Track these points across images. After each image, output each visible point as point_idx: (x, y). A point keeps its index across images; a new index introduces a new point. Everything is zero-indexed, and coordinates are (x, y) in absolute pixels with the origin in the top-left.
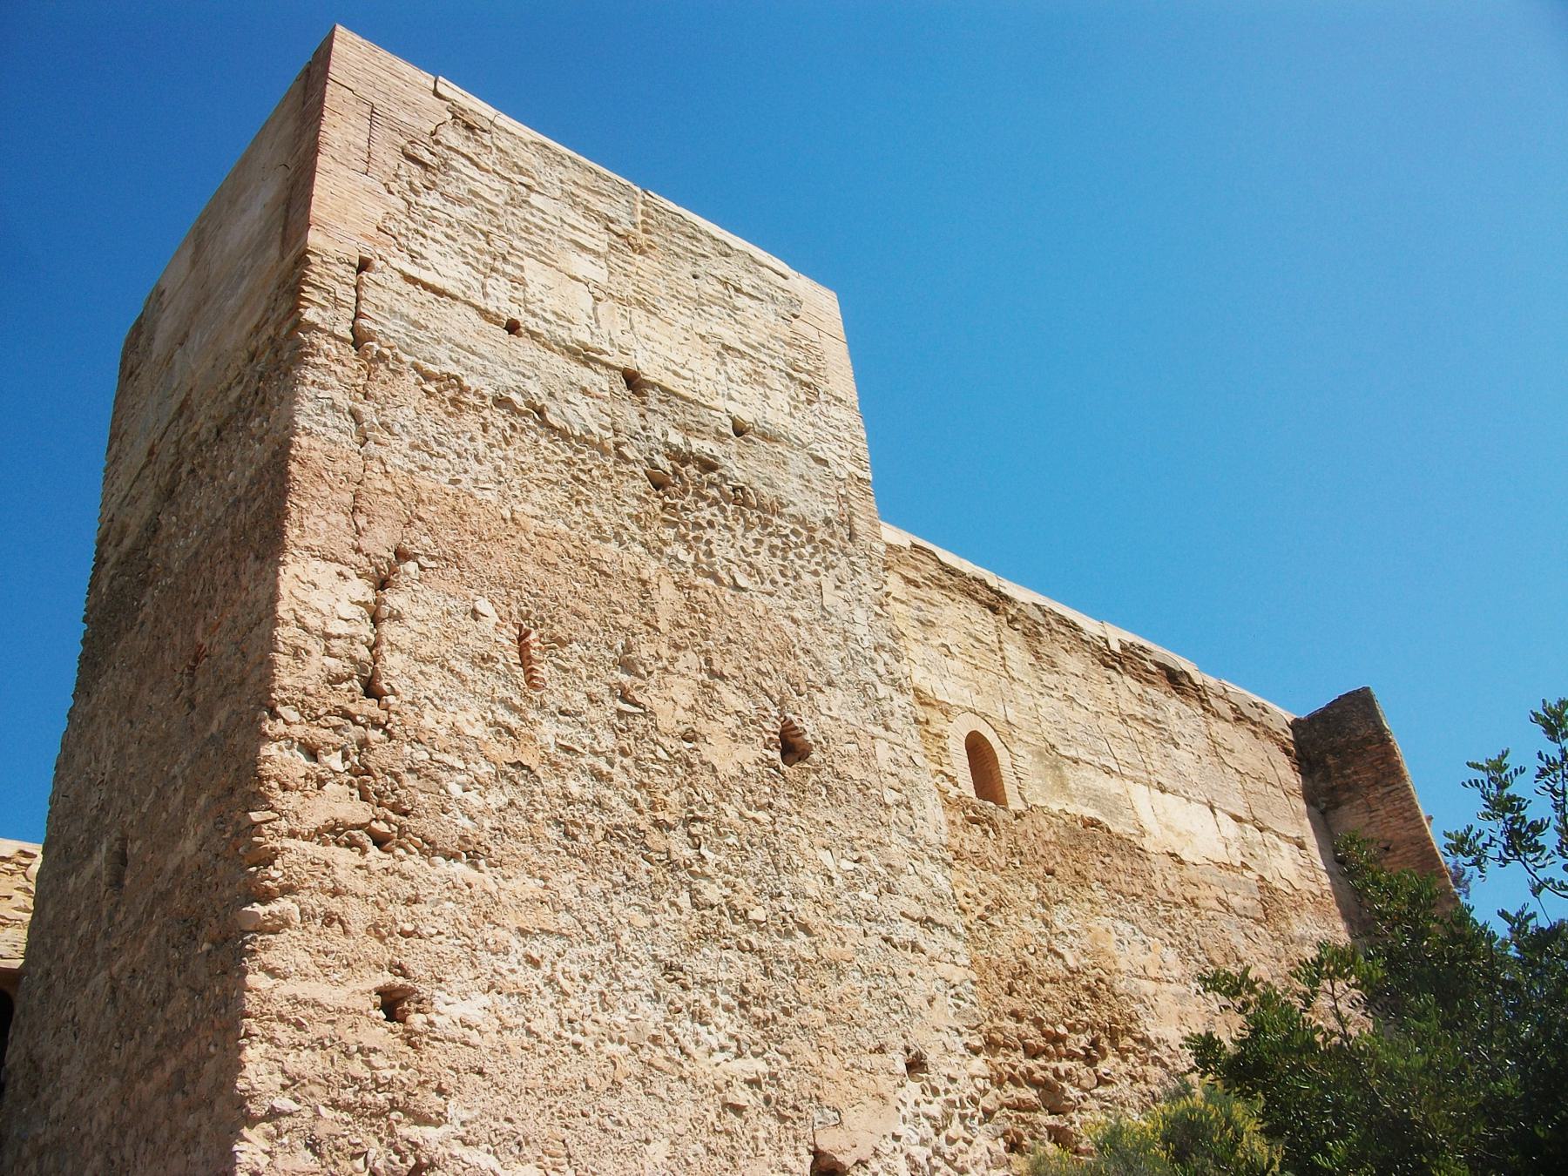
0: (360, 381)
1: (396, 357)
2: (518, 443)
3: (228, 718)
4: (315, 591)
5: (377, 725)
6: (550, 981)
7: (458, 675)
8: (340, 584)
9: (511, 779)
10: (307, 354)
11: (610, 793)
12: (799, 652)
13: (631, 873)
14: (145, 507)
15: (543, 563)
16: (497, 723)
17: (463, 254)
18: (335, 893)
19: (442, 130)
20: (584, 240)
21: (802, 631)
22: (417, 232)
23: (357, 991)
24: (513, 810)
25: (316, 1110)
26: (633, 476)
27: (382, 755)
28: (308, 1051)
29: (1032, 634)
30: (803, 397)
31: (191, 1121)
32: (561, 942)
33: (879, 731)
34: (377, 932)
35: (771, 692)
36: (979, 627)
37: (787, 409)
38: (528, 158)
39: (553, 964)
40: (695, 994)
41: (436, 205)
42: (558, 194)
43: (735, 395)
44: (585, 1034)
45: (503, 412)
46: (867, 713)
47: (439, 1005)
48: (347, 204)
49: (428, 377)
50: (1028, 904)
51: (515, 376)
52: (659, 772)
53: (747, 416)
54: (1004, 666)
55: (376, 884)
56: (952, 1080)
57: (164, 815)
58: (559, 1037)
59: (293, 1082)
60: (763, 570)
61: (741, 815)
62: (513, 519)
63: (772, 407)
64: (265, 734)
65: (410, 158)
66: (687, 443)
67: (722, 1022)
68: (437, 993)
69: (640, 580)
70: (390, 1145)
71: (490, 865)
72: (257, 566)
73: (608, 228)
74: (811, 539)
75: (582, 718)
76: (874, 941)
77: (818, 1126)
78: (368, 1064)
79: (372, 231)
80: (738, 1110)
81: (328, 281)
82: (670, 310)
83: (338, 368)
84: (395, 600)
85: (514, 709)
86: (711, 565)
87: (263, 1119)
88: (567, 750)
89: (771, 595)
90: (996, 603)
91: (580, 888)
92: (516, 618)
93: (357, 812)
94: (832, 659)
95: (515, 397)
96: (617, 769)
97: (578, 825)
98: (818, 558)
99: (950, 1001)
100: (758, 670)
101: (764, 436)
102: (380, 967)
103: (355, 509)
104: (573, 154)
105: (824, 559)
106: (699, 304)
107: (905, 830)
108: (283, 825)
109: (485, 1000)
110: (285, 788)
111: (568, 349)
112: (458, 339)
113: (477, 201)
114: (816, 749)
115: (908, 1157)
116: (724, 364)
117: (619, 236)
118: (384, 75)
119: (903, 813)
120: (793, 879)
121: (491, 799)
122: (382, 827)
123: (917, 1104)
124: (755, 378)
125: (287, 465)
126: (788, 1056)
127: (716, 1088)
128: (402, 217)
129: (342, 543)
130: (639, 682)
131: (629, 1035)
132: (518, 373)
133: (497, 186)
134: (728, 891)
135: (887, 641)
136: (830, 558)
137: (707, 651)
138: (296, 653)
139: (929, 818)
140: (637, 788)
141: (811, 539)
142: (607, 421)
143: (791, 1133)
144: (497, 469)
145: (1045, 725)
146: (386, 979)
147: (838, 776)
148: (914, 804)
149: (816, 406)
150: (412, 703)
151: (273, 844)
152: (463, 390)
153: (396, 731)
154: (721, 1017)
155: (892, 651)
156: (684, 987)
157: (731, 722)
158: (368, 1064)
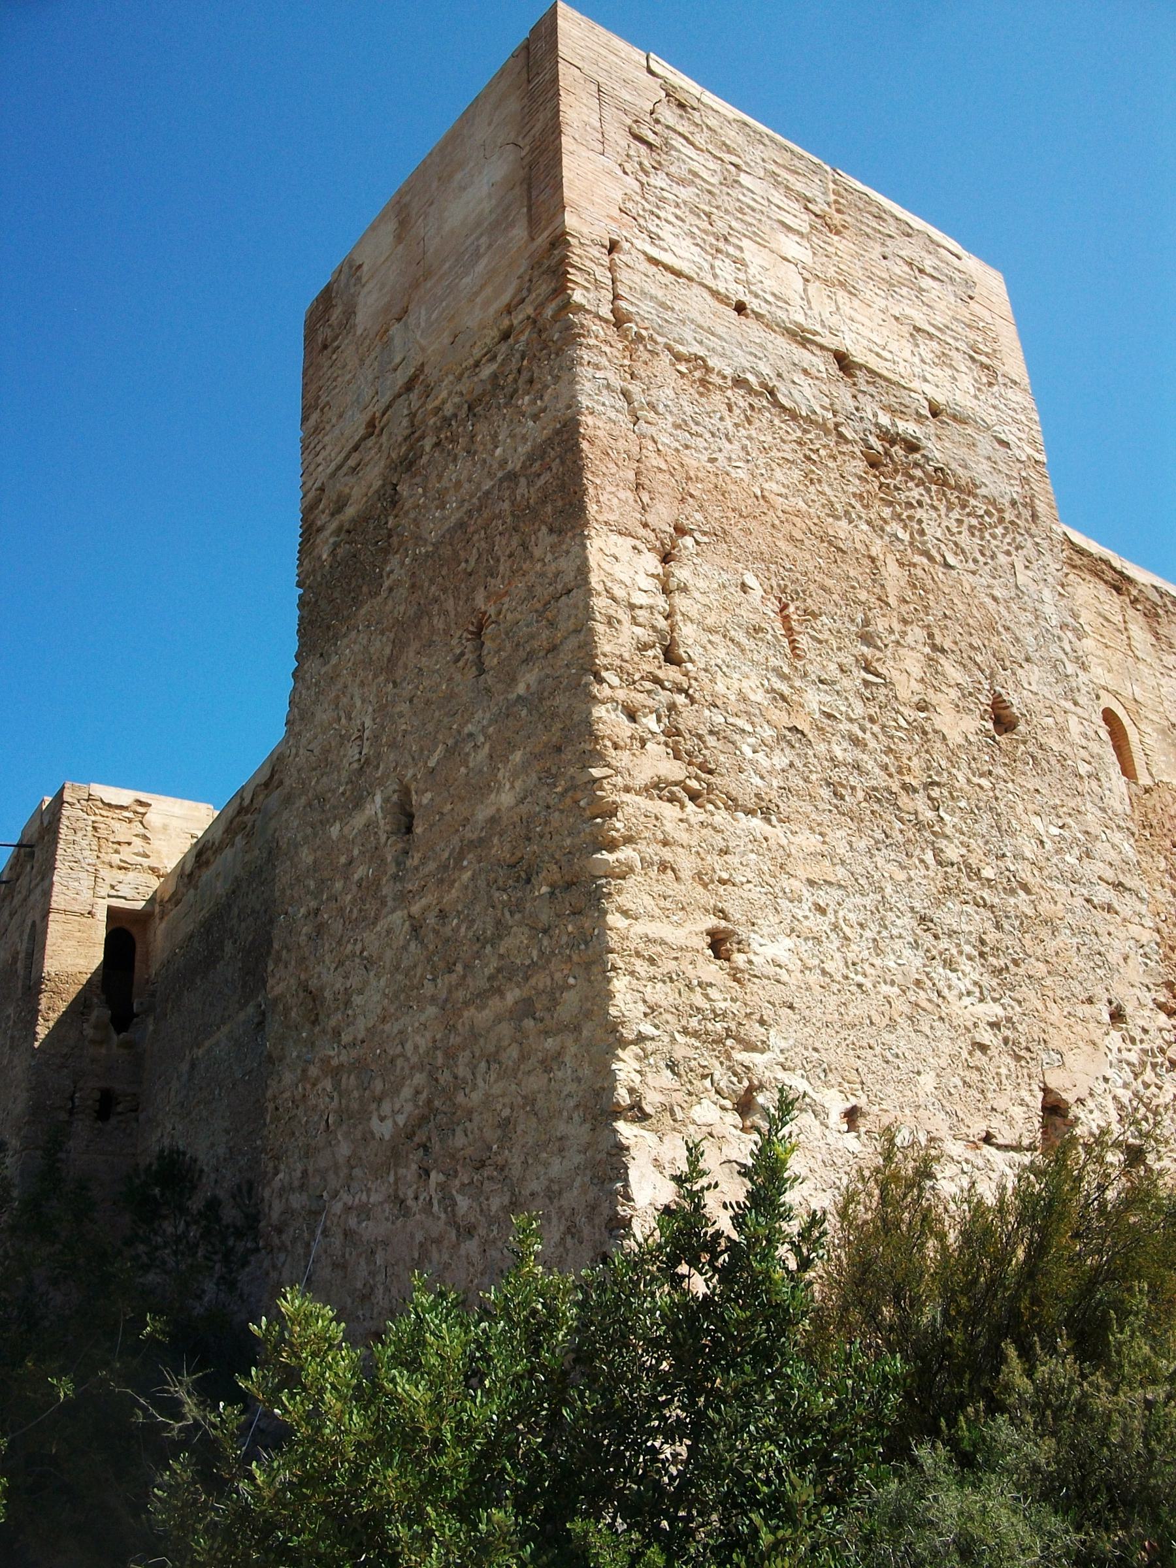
0: (626, 362)
1: (651, 337)
2: (757, 424)
3: (540, 682)
4: (617, 564)
5: (681, 690)
6: (835, 927)
7: (738, 645)
8: (636, 557)
9: (789, 743)
10: (580, 335)
11: (866, 757)
12: (1001, 629)
13: (888, 832)
14: (373, 475)
15: (792, 539)
16: (774, 690)
17: (692, 235)
18: (665, 843)
19: (660, 109)
20: (789, 220)
21: (1001, 609)
22: (652, 213)
23: (691, 932)
24: (792, 771)
25: (672, 1036)
26: (853, 455)
27: (688, 718)
28: (660, 984)
29: (1152, 615)
30: (985, 380)
31: (550, 1043)
32: (840, 892)
33: (1069, 705)
34: (701, 879)
35: (983, 666)
36: (1107, 607)
37: (972, 391)
38: (732, 136)
39: (836, 912)
40: (944, 943)
41: (664, 186)
42: (762, 174)
43: (929, 377)
44: (865, 975)
45: (742, 392)
46: (1059, 689)
47: (755, 946)
48: (593, 187)
49: (678, 357)
50: (1158, 874)
51: (751, 358)
52: (901, 739)
53: (940, 398)
54: (1129, 645)
55: (696, 836)
56: (1145, 1031)
57: (463, 770)
58: (847, 978)
59: (652, 1010)
60: (967, 548)
61: (969, 781)
62: (763, 497)
63: (957, 389)
64: (595, 697)
65: (638, 138)
66: (894, 424)
67: (968, 969)
68: (752, 935)
69: (869, 557)
70: (729, 1068)
71: (780, 821)
72: (554, 538)
73: (807, 208)
74: (1001, 520)
75: (837, 687)
76: (1079, 901)
77: (1046, 1067)
78: (706, 996)
79: (615, 213)
80: (983, 1048)
81: (588, 263)
82: (868, 291)
83: (607, 349)
84: (682, 573)
85: (784, 677)
86: (924, 543)
87: (632, 1043)
88: (829, 716)
89: (974, 573)
90: (1120, 584)
91: (850, 843)
92: (777, 592)
93: (675, 770)
94: (1028, 636)
95: (751, 378)
96: (868, 736)
97: (843, 786)
98: (1008, 540)
99: (1140, 959)
100: (971, 645)
101: (954, 418)
102: (707, 910)
103: (639, 486)
104: (770, 132)
105: (1014, 539)
106: (891, 285)
107: (1097, 800)
108: (619, 780)
109: (788, 943)
110: (616, 747)
111: (787, 330)
112: (696, 320)
113: (697, 181)
114: (1022, 721)
115: (1114, 1098)
116: (917, 345)
117: (817, 216)
118: (604, 52)
119: (1094, 784)
120: (1013, 841)
121: (776, 760)
122: (693, 784)
123: (1120, 1050)
124: (943, 360)
125: (577, 444)
126: (1019, 1003)
127: (966, 1028)
128: (638, 198)
129: (632, 520)
130: (879, 654)
131: (899, 978)
132: (751, 353)
133: (711, 165)
134: (964, 851)
135: (1070, 620)
136: (1019, 538)
137: (929, 626)
138: (610, 621)
139: (1114, 789)
140: (886, 754)
141: (1001, 520)
142: (826, 402)
143: (1025, 1071)
144: (744, 448)
145: (1166, 704)
146: (712, 922)
147: (1041, 747)
148: (1102, 775)
149: (996, 388)
150: (706, 670)
151: (613, 798)
152: (708, 370)
153: (697, 696)
154: (965, 965)
155: (1074, 630)
156: (936, 937)
157: (954, 693)
158: (706, 996)
